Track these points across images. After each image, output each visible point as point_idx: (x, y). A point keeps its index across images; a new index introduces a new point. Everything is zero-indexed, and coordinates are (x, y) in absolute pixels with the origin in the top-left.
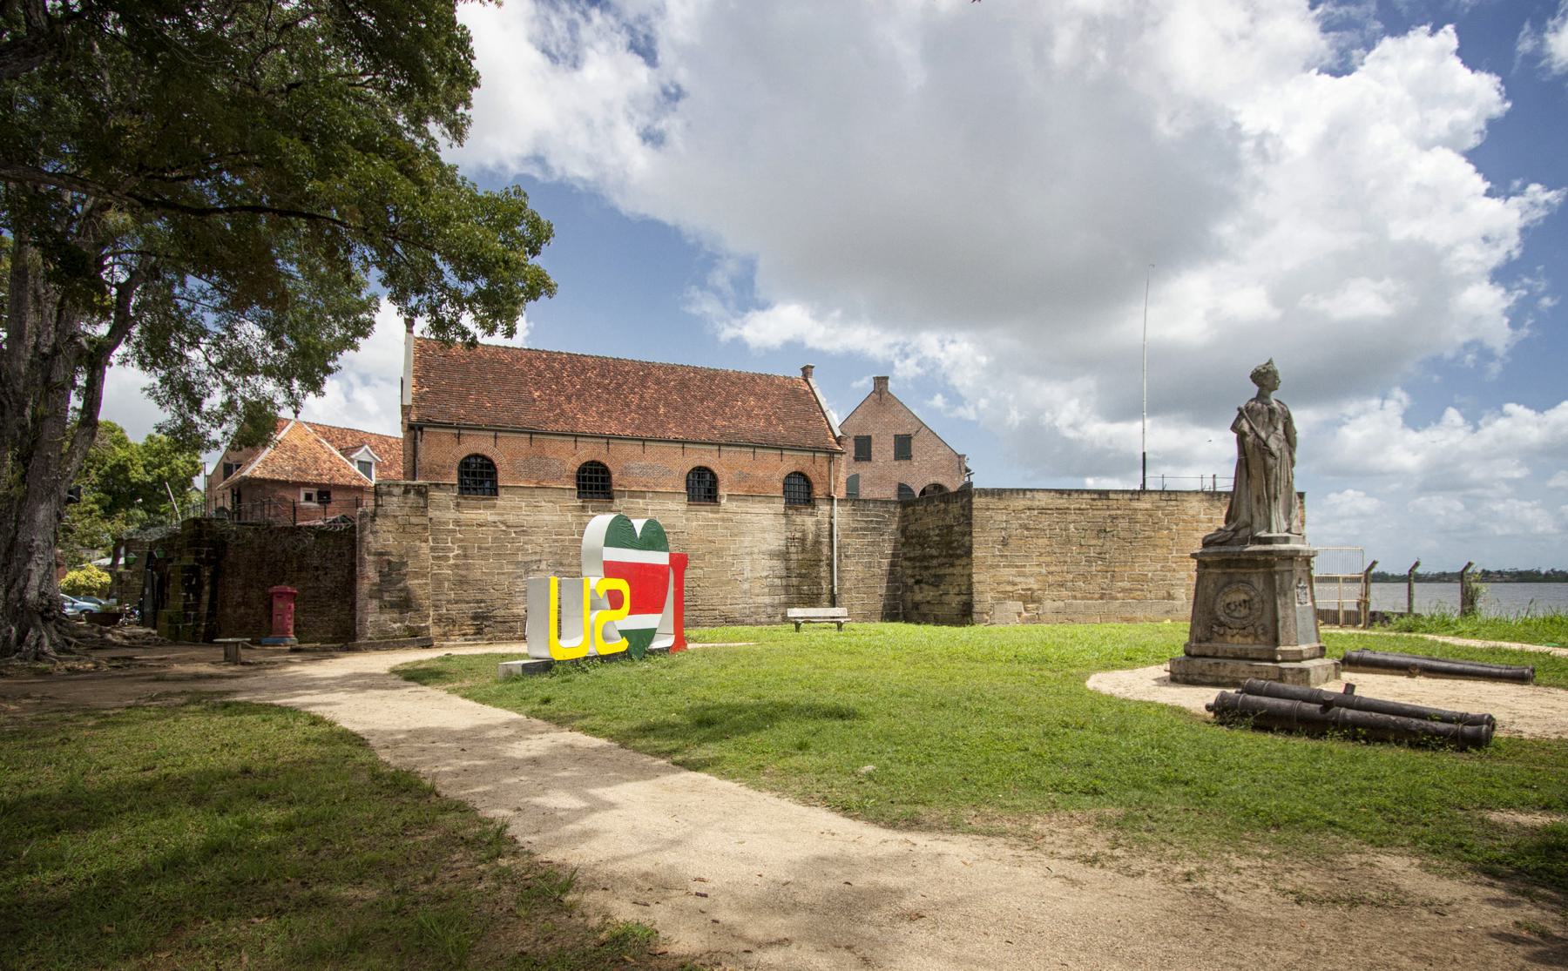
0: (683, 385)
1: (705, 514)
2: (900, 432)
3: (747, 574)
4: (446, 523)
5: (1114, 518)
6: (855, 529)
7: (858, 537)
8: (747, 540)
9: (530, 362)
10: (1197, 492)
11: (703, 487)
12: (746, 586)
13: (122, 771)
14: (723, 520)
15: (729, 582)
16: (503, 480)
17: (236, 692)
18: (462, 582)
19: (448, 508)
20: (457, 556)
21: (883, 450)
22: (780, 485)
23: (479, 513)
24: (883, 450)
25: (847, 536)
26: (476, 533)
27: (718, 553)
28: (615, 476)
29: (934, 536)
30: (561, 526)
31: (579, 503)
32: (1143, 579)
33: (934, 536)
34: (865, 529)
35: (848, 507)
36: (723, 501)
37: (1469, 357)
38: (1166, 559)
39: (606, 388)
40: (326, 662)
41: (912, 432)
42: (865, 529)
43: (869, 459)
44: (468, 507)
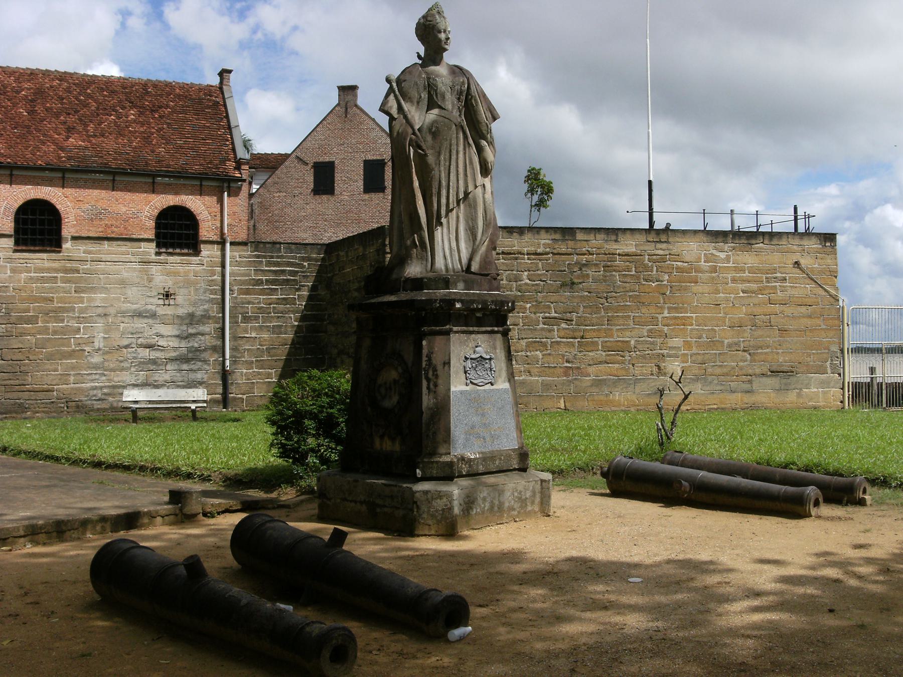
0: (40, 93)
1: (41, 260)
5: (582, 266)
6: (259, 282)
7: (262, 292)
8: (99, 297)
10: (696, 232)
12: (96, 359)
13: (879, 586)
14: (66, 271)
15: (71, 354)
17: (5, 515)
22: (152, 224)
25: (247, 292)
27: (56, 314)
32: (622, 348)
34: (273, 282)
35: (247, 252)
36: (67, 245)
38: (654, 321)
40: (447, 484)
42: (273, 282)
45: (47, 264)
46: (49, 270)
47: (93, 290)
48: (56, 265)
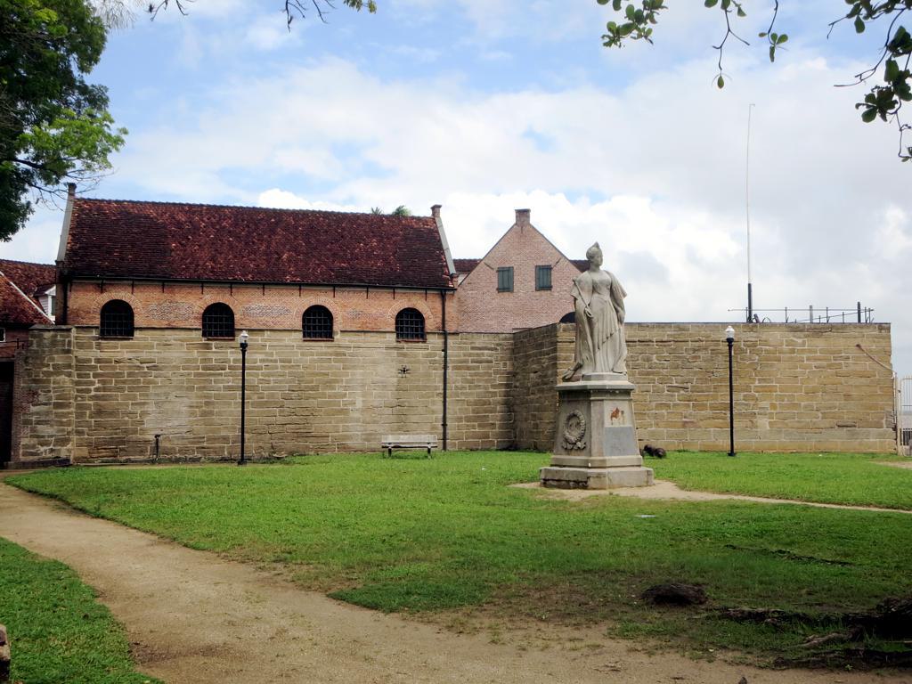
1: (320, 347)
2: (540, 263)
3: (359, 405)
4: (90, 360)
9: (318, 218)
11: (318, 324)
16: (139, 321)
18: (99, 412)
19: (90, 347)
20: (97, 389)
21: (525, 282)
23: (118, 350)
24: (525, 282)
26: (114, 368)
28: (237, 317)
29: (193, 398)
30: (188, 361)
31: (204, 340)
33: (193, 398)
36: (337, 337)
37: (15, 75)
39: (238, 237)
41: (552, 263)
43: (549, 288)
44: (109, 347)
45: (324, 350)
46: (326, 354)
47: (354, 367)
48: (330, 350)
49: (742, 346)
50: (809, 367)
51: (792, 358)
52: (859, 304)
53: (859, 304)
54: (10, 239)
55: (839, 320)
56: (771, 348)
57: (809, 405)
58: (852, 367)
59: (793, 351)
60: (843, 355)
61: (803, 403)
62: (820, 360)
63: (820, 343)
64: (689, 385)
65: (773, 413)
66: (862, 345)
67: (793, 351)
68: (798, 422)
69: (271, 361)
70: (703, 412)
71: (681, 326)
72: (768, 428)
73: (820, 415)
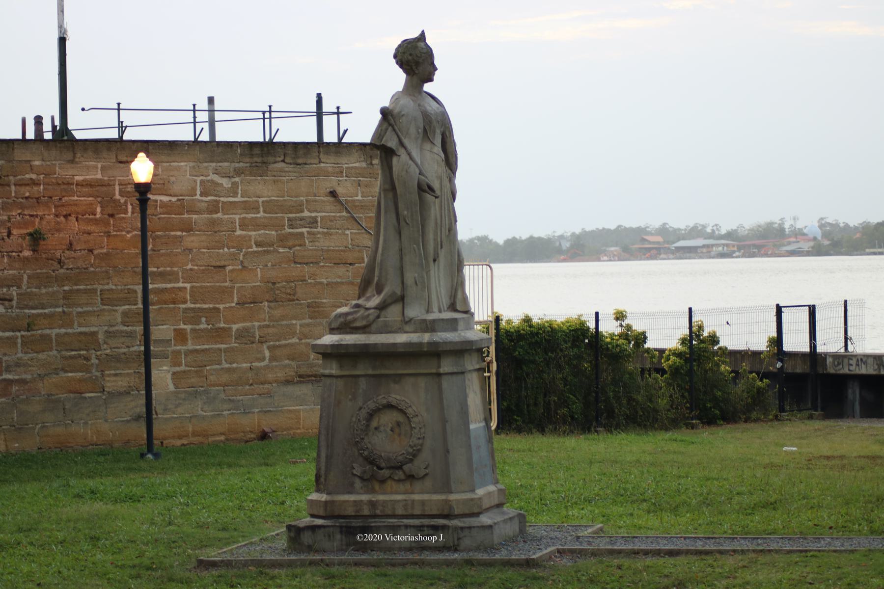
49: (117, 197)
50: (241, 243)
51: (213, 222)
52: (319, 98)
53: (319, 98)
54: (620, 316)
55: (253, 133)
56: (174, 199)
57: (246, 330)
58: (323, 243)
59: (214, 208)
60: (306, 214)
61: (235, 327)
62: (265, 227)
63: (262, 189)
64: (14, 291)
65: (179, 352)
66: (340, 190)
67: (214, 208)
68: (229, 370)
69: (403, 564)
70: (42, 356)
71: (452, 232)
72: (171, 387)
73: (267, 354)
